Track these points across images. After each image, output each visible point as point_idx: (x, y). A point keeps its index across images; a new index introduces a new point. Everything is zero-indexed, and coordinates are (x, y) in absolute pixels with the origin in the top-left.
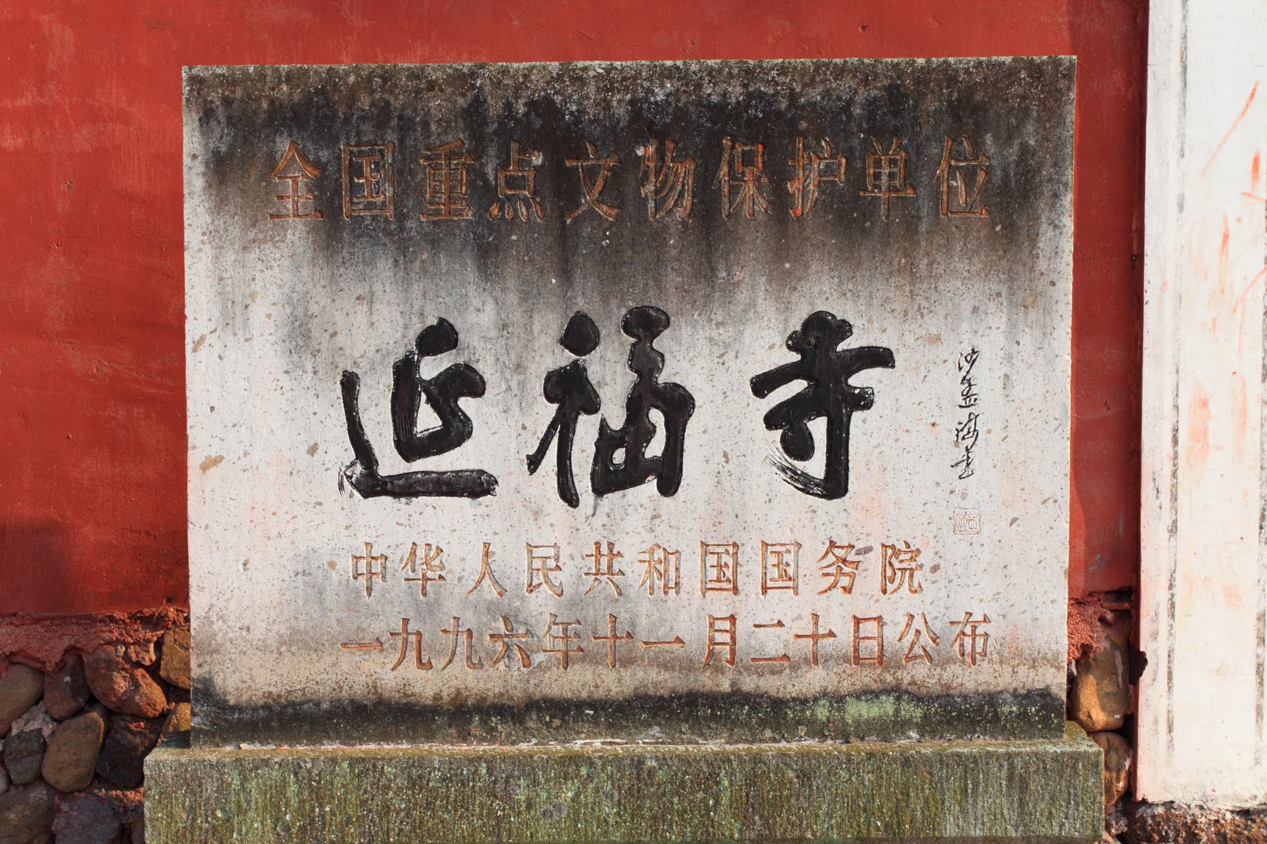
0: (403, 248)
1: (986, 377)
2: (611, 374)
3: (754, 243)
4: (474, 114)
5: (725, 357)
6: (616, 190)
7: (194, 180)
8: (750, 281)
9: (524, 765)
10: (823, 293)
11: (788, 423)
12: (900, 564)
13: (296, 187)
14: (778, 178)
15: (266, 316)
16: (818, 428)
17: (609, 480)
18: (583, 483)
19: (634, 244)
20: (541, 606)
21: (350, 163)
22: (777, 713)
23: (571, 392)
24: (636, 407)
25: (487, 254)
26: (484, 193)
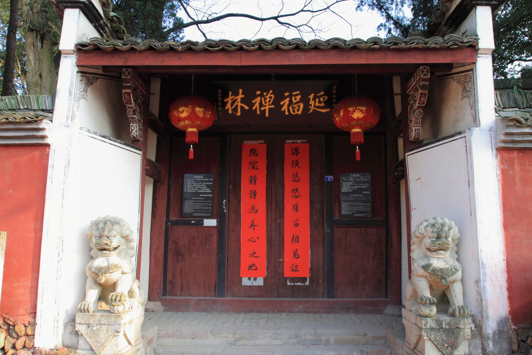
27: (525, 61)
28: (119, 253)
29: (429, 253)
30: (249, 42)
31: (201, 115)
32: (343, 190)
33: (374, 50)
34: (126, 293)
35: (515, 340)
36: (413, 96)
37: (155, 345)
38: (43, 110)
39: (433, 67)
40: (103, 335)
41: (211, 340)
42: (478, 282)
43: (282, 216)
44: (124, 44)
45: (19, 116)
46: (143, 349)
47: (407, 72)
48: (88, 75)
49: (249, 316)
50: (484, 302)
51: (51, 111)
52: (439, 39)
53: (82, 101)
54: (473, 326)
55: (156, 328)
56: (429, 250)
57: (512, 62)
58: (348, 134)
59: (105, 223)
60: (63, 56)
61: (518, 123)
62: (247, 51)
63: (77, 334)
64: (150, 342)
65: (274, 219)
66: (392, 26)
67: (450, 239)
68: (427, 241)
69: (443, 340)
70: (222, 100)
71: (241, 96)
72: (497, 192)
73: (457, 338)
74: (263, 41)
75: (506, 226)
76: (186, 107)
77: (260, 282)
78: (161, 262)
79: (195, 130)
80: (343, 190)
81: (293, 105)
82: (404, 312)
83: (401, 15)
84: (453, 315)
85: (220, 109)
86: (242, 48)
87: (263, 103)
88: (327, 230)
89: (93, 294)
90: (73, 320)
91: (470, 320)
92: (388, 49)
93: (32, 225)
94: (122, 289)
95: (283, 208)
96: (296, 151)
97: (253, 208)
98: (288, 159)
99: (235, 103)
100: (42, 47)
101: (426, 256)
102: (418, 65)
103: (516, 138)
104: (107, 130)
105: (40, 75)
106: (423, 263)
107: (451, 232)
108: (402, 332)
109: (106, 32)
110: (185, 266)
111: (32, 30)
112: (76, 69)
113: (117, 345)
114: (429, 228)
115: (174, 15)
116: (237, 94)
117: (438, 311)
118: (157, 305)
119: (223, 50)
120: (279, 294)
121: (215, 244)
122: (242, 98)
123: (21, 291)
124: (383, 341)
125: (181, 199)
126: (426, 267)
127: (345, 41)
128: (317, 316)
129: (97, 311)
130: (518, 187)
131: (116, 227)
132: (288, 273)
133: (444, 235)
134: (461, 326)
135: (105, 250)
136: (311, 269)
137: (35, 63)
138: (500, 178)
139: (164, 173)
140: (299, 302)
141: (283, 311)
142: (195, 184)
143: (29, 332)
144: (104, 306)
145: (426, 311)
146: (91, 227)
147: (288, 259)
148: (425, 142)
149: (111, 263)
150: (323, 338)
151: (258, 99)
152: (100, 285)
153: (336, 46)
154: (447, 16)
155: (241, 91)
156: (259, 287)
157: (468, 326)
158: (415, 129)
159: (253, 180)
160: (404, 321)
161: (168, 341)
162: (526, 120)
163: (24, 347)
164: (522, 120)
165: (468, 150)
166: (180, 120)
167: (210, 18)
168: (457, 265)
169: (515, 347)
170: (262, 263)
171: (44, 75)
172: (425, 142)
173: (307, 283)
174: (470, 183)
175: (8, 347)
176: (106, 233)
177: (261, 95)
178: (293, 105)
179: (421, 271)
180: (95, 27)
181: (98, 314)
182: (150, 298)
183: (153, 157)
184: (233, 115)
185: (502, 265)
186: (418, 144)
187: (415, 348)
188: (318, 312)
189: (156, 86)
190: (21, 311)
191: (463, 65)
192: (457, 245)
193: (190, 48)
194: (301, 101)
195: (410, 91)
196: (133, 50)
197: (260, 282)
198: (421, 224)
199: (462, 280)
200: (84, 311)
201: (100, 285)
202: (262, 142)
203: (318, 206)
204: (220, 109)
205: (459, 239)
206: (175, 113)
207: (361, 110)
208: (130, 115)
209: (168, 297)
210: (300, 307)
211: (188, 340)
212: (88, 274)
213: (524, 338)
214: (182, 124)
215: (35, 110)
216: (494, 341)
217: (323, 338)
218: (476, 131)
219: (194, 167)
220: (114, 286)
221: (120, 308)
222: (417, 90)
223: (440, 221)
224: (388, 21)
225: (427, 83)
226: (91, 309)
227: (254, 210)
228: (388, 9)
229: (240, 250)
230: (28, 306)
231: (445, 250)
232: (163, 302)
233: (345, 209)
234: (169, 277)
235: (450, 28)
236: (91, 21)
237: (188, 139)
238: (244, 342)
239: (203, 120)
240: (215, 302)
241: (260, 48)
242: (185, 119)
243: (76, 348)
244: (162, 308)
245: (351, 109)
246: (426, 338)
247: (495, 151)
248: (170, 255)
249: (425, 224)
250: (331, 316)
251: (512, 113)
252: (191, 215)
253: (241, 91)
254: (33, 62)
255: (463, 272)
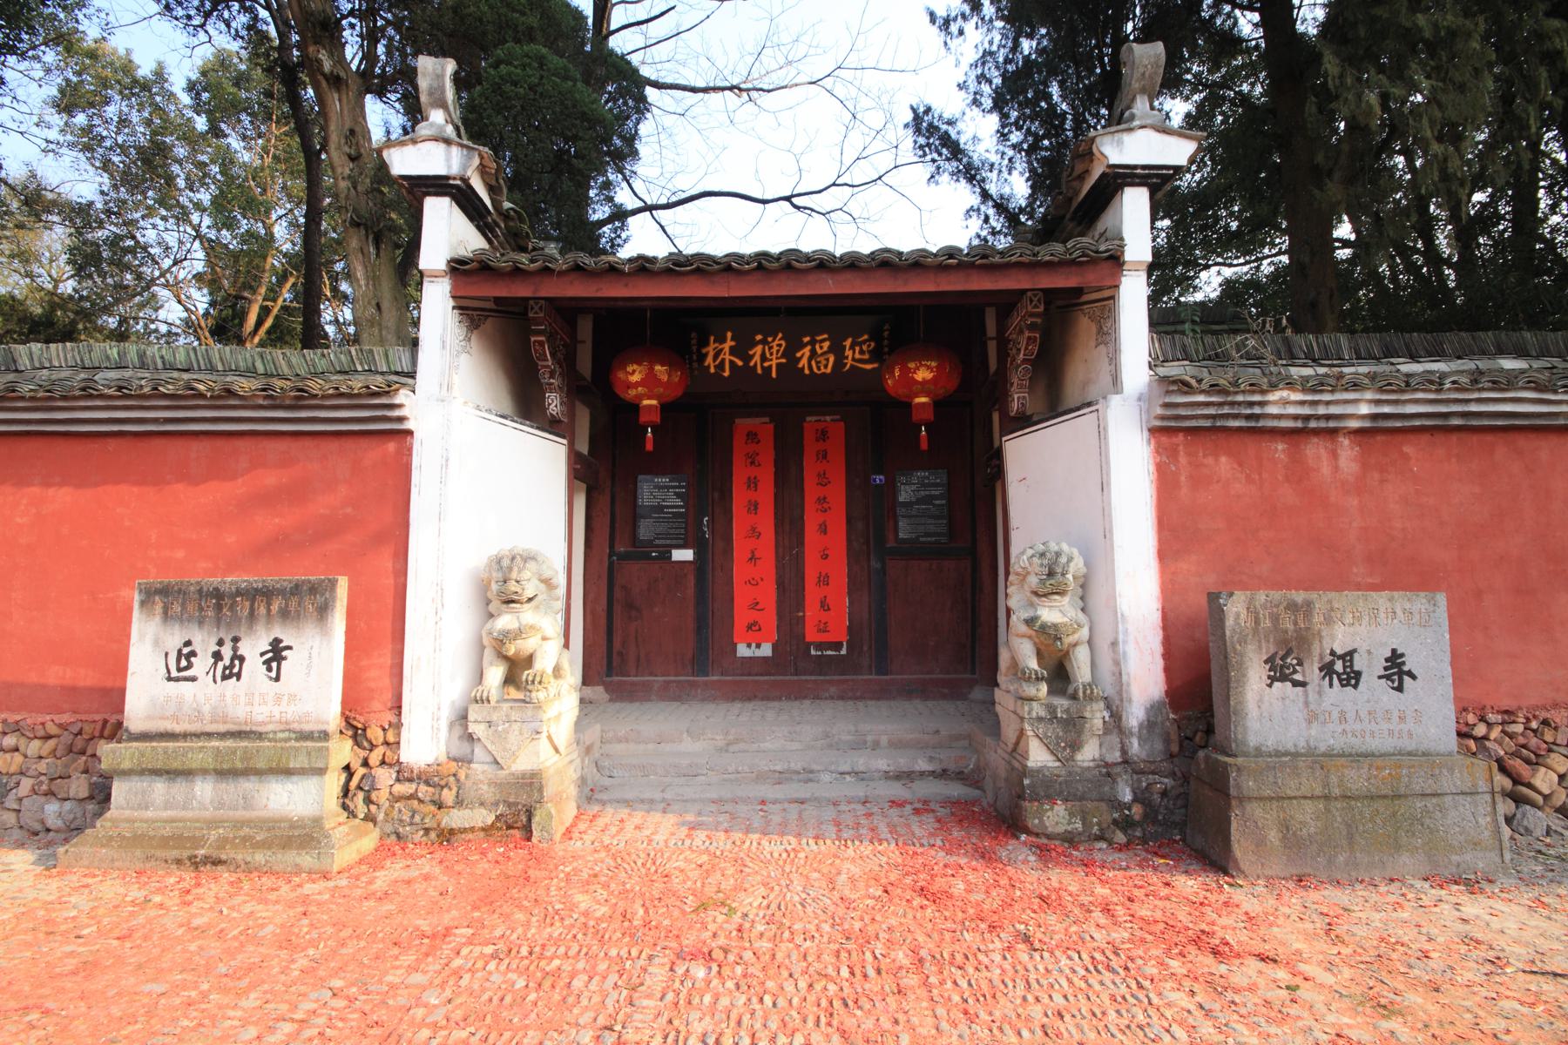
0: (182, 621)
1: (315, 652)
2: (227, 652)
3: (263, 621)
4: (200, 591)
5: (254, 647)
6: (232, 608)
7: (136, 606)
8: (260, 628)
9: (191, 749)
10: (277, 632)
11: (267, 663)
12: (293, 698)
13: (159, 608)
14: (269, 604)
15: (149, 638)
16: (274, 665)
17: (224, 678)
18: (219, 678)
19: (236, 620)
20: (206, 709)
21: (170, 599)
22: (260, 736)
23: (217, 656)
24: (232, 660)
25: (201, 623)
26: (201, 609)
27: (1231, 265)
28: (537, 607)
29: (1035, 599)
30: (741, 256)
31: (665, 378)
32: (901, 499)
33: (949, 267)
34: (549, 671)
35: (1174, 737)
36: (1016, 343)
37: (596, 754)
38: (397, 373)
39: (1049, 295)
40: (513, 738)
41: (688, 745)
42: (1114, 644)
43: (801, 543)
44: (532, 261)
45: (357, 384)
46: (578, 761)
47: (1007, 302)
48: (471, 312)
49: (750, 705)
50: (1124, 678)
51: (412, 375)
52: (1058, 247)
53: (464, 357)
54: (1107, 715)
55: (598, 727)
56: (1036, 593)
57: (1207, 267)
58: (909, 405)
59: (513, 559)
60: (426, 279)
61: (1184, 386)
62: (738, 272)
63: (470, 738)
64: (588, 750)
65: (785, 550)
66: (991, 212)
67: (1070, 576)
68: (1033, 581)
69: (1057, 737)
70: (699, 351)
71: (729, 343)
72: (1149, 500)
73: (1080, 733)
74: (764, 255)
75: (1163, 555)
76: (639, 364)
77: (766, 650)
78: (603, 622)
79: (654, 402)
80: (901, 499)
81: (816, 358)
82: (998, 694)
83: (1006, 191)
84: (1074, 697)
85: (695, 365)
86: (729, 266)
87: (768, 355)
88: (875, 564)
89: (495, 674)
90: (463, 717)
91: (1102, 705)
92: (972, 265)
93: (390, 565)
94: (544, 663)
95: (802, 530)
96: (823, 435)
97: (753, 529)
98: (811, 447)
99: (720, 354)
100: (378, 255)
101: (1032, 605)
102: (1024, 292)
103: (1183, 412)
104: (507, 405)
105: (378, 306)
106: (1026, 615)
107: (1072, 565)
108: (995, 729)
109: (496, 237)
110: (645, 630)
111: (358, 225)
112: (451, 303)
113: (537, 754)
114: (1035, 560)
115: (610, 199)
116: (723, 341)
117: (1050, 692)
118: (598, 692)
119: (698, 270)
120: (796, 672)
121: (690, 590)
122: (731, 348)
123: (373, 673)
124: (966, 743)
125: (635, 515)
126: (1030, 622)
127: (900, 254)
128: (861, 704)
129: (502, 700)
130: (1184, 491)
131: (531, 565)
132: (811, 635)
133: (1059, 570)
134: (1087, 715)
135: (513, 601)
136: (850, 628)
137: (367, 285)
138: (1153, 477)
139: (603, 476)
140: (830, 682)
141: (805, 697)
142: (657, 492)
143: (391, 739)
144: (514, 693)
145: (1030, 690)
146: (489, 566)
147: (811, 612)
148: (1035, 418)
149: (524, 622)
150: (869, 738)
151: (759, 349)
152: (506, 658)
153: (886, 262)
154: (1075, 204)
155: (729, 335)
156: (765, 659)
157: (1098, 715)
158: (1018, 399)
159: (752, 483)
160: (998, 708)
161: (618, 748)
162: (1200, 381)
163: (383, 763)
164: (1193, 382)
165: (1101, 431)
166: (629, 386)
167: (674, 199)
168: (1081, 617)
169: (1175, 748)
170: (770, 619)
171: (385, 305)
172: (1035, 418)
173: (844, 652)
174: (1104, 487)
175: (356, 764)
176: (514, 575)
177: (764, 342)
178: (816, 358)
179: (1023, 628)
180: (478, 227)
181: (506, 706)
182: (586, 681)
183: (584, 448)
184: (718, 375)
185: (1155, 617)
186: (1023, 422)
187: (1014, 750)
188: (861, 698)
189: (585, 328)
190: (376, 705)
191: (1100, 289)
192: (1082, 586)
193: (643, 266)
194: (830, 350)
195: (1011, 333)
196: (546, 271)
197: (766, 650)
198: (1023, 553)
199: (1090, 642)
200: (481, 700)
201: (506, 658)
202: (767, 419)
203: (860, 525)
204: (695, 365)
205: (1085, 576)
206: (621, 375)
207: (928, 367)
208: (545, 379)
209: (616, 679)
210: (833, 690)
211: (651, 746)
212: (486, 641)
213: (1189, 734)
214: (632, 392)
215: (382, 373)
216: (1140, 738)
217: (869, 738)
218: (1115, 400)
219: (654, 465)
220: (529, 661)
221: (541, 695)
222: (1021, 332)
223: (1054, 547)
224: (983, 203)
225: (1039, 320)
226: (493, 699)
227: (754, 533)
228: (983, 180)
229: (732, 599)
230: (388, 696)
231: (1062, 593)
232: (609, 688)
233: (905, 530)
234: (617, 645)
235: (1080, 224)
236: (471, 219)
237: (643, 418)
238: (742, 746)
239: (667, 385)
240: (693, 685)
241: (760, 267)
242: (637, 384)
243: (470, 762)
244: (606, 696)
245: (912, 365)
246: (1030, 733)
247: (1146, 433)
248: (617, 609)
249: (1030, 552)
250: (883, 704)
251: (1174, 370)
252: (650, 544)
253: (729, 335)
254: (362, 283)
255: (1091, 630)
